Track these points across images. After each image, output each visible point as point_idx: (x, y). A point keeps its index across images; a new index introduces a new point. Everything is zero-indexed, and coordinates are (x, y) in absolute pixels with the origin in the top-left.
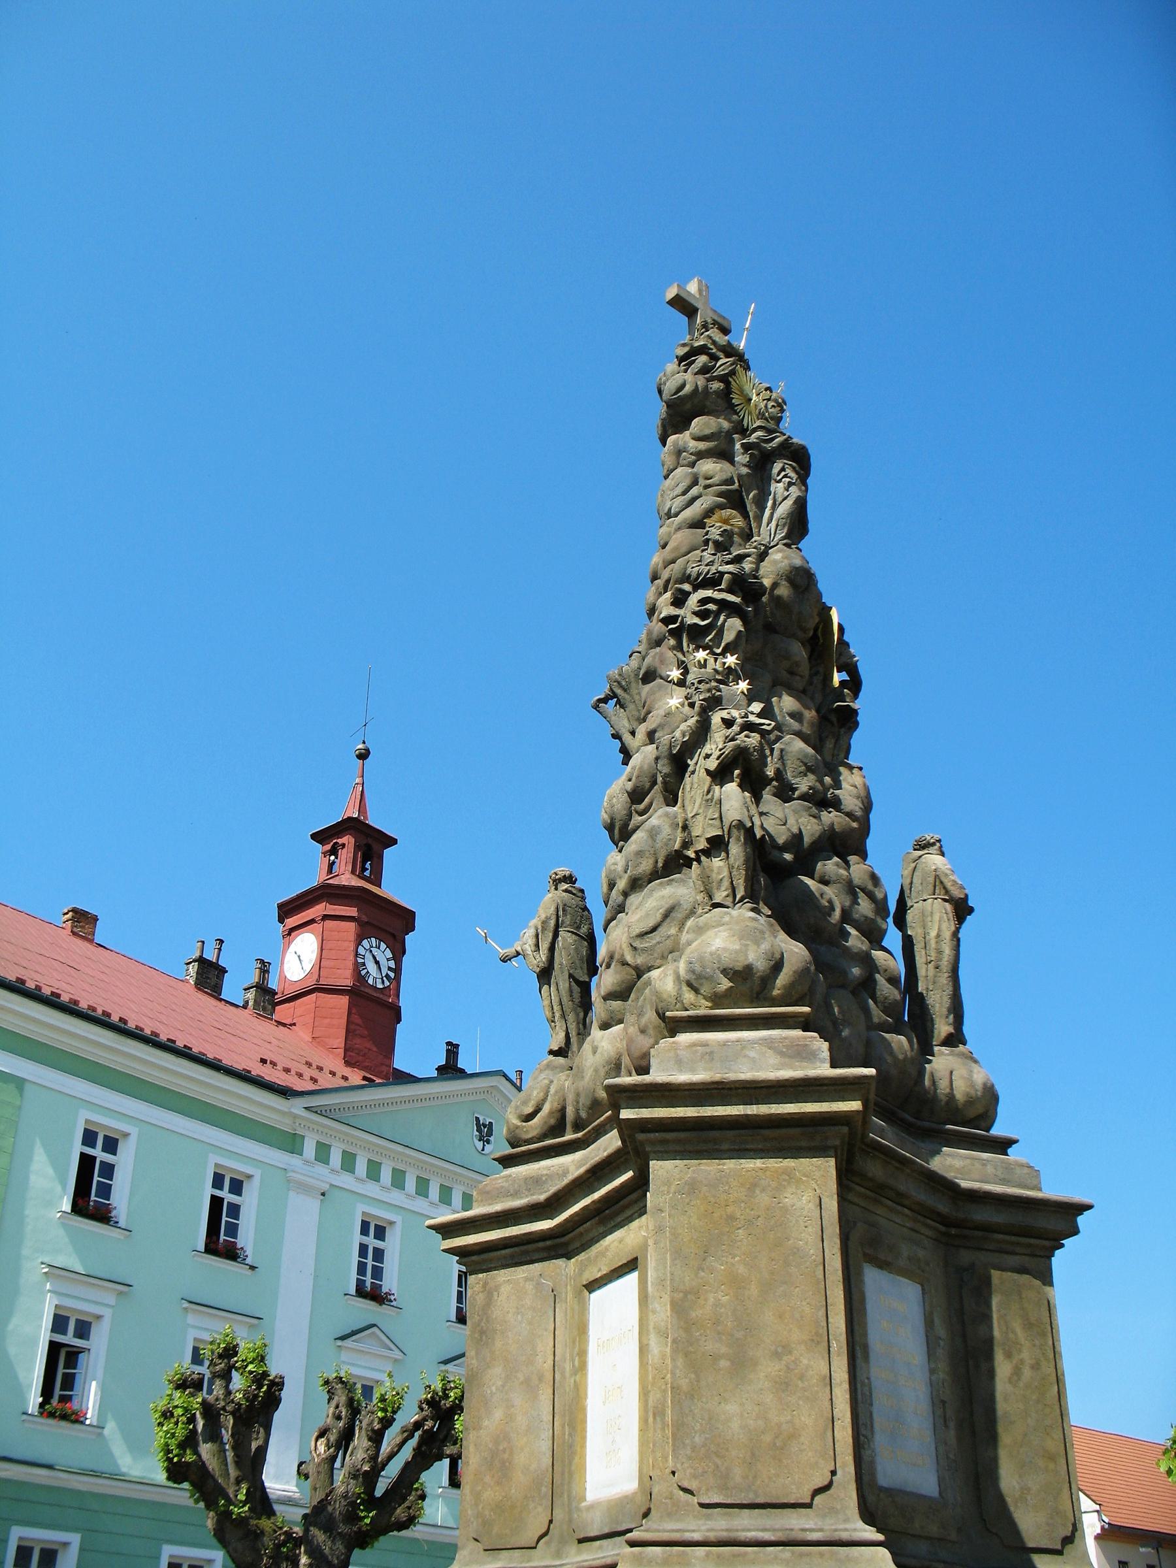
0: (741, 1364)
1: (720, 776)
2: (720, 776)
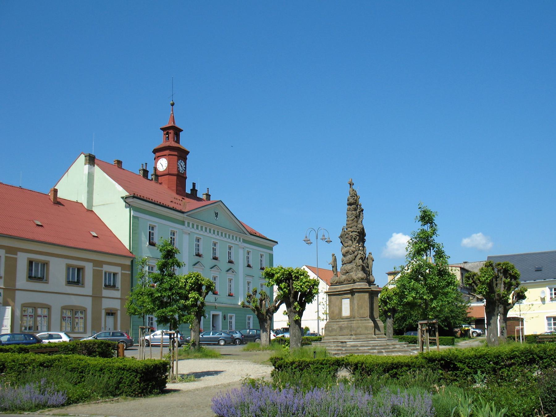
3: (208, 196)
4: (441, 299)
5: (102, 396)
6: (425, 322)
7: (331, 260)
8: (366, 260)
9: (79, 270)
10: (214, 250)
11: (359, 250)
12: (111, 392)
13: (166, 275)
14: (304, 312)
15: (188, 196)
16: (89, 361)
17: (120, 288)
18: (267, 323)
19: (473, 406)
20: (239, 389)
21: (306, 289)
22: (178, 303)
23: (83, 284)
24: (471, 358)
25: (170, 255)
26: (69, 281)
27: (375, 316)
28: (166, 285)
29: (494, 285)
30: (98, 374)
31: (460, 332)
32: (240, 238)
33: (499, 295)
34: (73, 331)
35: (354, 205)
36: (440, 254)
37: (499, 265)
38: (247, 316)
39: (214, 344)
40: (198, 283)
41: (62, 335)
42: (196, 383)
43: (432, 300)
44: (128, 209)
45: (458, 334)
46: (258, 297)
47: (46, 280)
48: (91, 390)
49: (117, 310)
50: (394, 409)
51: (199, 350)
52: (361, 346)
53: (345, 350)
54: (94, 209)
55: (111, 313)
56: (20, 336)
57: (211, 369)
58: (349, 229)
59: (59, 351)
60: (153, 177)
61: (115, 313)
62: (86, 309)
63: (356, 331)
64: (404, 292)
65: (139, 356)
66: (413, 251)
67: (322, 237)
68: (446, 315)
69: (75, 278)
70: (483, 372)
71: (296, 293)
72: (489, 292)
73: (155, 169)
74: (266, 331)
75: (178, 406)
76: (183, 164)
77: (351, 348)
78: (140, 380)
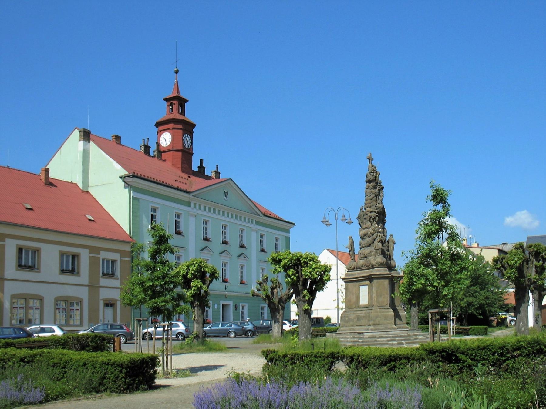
3: (218, 173)
4: (453, 286)
5: (84, 393)
6: (436, 310)
7: (348, 243)
8: (387, 243)
9: (74, 257)
10: (224, 233)
11: (379, 232)
12: (94, 388)
15: (194, 174)
16: (71, 356)
17: (119, 276)
18: (279, 313)
19: (466, 401)
20: (222, 384)
21: (316, 276)
22: (173, 291)
23: (78, 273)
24: (474, 349)
25: (162, 241)
26: (63, 270)
27: (396, 305)
28: (157, 274)
30: (81, 370)
31: (496, 320)
32: (252, 220)
33: (530, 280)
34: (68, 325)
35: (374, 183)
36: (453, 237)
37: (530, 246)
38: (261, 305)
39: (224, 337)
40: (201, 270)
41: (55, 328)
42: (190, 378)
44: (127, 190)
45: (494, 323)
46: (269, 285)
47: (38, 269)
48: (72, 386)
49: (116, 300)
50: (381, 404)
51: (203, 343)
52: (380, 337)
53: (362, 342)
54: (90, 190)
55: (109, 304)
56: (9, 330)
57: (212, 364)
58: (368, 209)
59: (48, 346)
60: (156, 153)
61: (114, 304)
62: (82, 299)
64: (413, 279)
65: (131, 351)
66: (424, 233)
67: (341, 218)
69: (70, 266)
70: (483, 365)
71: (306, 280)
72: (519, 277)
73: (158, 144)
75: (163, 403)
76: (189, 138)
77: (369, 340)
78: (126, 375)
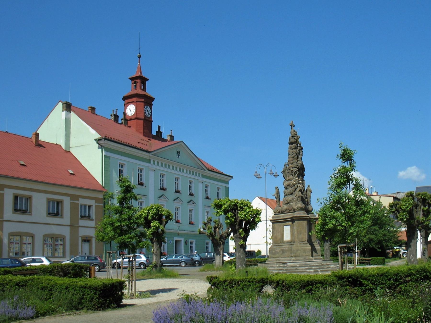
0: (301, 234)
1: (299, 191)
2: (299, 191)
3: (172, 137)
4: (358, 226)
5: (66, 310)
6: (344, 245)
7: (274, 192)
8: (305, 192)
9: (58, 203)
10: (177, 184)
11: (299, 183)
13: (125, 207)
14: (248, 238)
15: (153, 137)
16: (56, 281)
17: (94, 218)
18: (220, 247)
19: (368, 316)
20: (175, 303)
21: (249, 218)
22: (136, 230)
24: (374, 276)
25: (128, 190)
26: (50, 213)
27: (313, 241)
28: (124, 216)
29: (414, 212)
30: (64, 292)
31: (391, 253)
32: (199, 174)
33: (418, 221)
34: (54, 256)
35: (295, 144)
37: (419, 195)
38: (206, 241)
39: (177, 266)
41: (44, 259)
42: (150, 299)
43: (350, 226)
44: (100, 150)
45: (390, 255)
46: (212, 225)
47: (30, 212)
48: (57, 305)
49: (92, 237)
50: (301, 319)
51: (160, 271)
52: (300, 266)
53: (286, 270)
54: (72, 150)
55: (86, 240)
56: (7, 260)
57: (167, 287)
58: (290, 165)
59: (38, 273)
60: (123, 121)
61: (90, 240)
63: (295, 253)
64: (326, 220)
65: (103, 277)
66: (334, 184)
68: (380, 238)
69: (55, 210)
70: (381, 288)
71: (241, 221)
72: (410, 219)
73: (125, 114)
74: (220, 254)
76: (149, 109)
77: (292, 268)
